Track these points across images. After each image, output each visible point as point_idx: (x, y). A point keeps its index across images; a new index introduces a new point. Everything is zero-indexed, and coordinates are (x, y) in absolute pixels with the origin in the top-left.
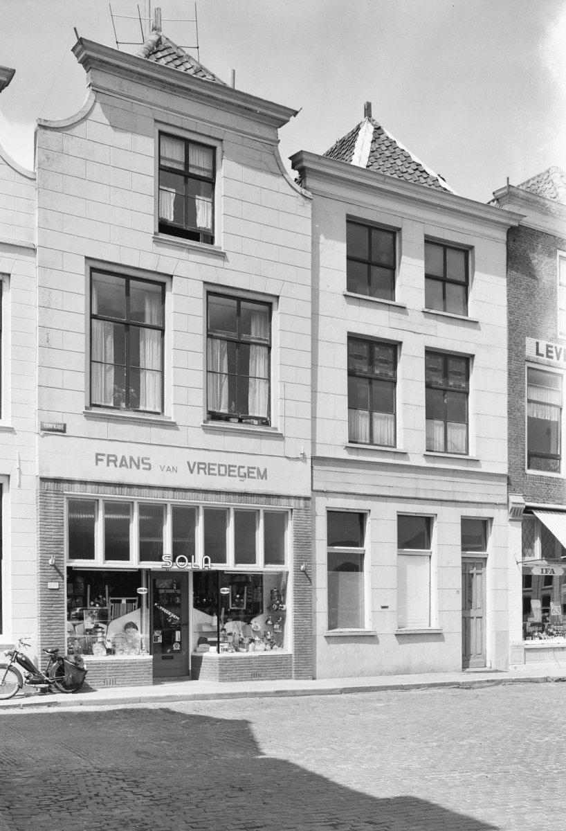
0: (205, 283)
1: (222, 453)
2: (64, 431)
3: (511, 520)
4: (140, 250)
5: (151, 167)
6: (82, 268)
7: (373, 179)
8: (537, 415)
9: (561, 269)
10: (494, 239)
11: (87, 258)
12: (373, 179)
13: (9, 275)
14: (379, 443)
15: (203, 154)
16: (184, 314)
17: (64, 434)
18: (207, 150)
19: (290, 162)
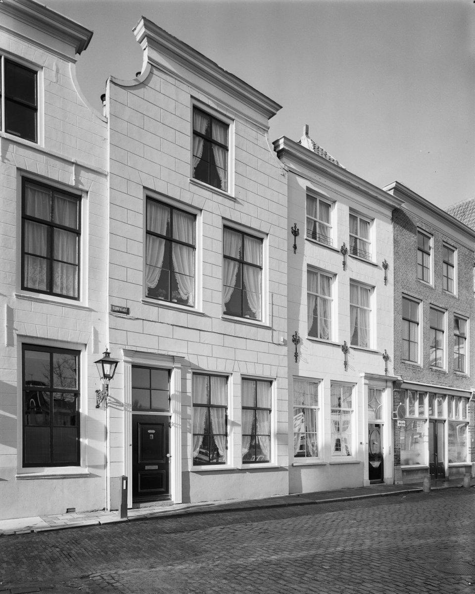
0: (223, 218)
1: (192, 330)
2: (128, 313)
3: (100, 342)
4: (179, 184)
5: (189, 131)
6: (141, 195)
7: (295, 149)
8: (150, 228)
9: (207, 99)
10: (386, 216)
11: (144, 187)
12: (295, 149)
13: (87, 192)
14: (38, 254)
15: (201, 117)
16: (206, 236)
17: (128, 316)
18: (208, 117)
19: (273, 146)
